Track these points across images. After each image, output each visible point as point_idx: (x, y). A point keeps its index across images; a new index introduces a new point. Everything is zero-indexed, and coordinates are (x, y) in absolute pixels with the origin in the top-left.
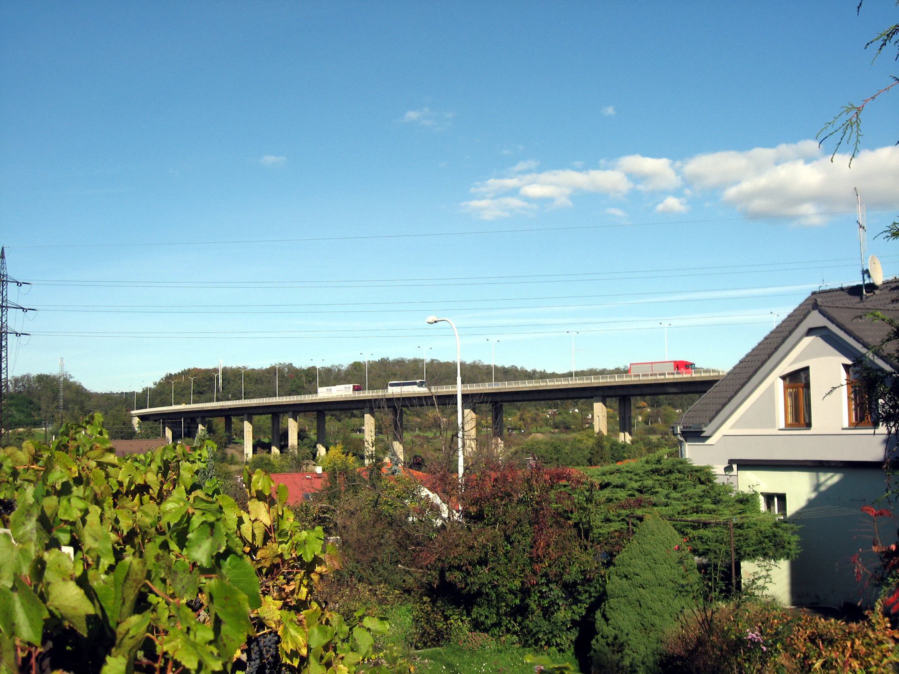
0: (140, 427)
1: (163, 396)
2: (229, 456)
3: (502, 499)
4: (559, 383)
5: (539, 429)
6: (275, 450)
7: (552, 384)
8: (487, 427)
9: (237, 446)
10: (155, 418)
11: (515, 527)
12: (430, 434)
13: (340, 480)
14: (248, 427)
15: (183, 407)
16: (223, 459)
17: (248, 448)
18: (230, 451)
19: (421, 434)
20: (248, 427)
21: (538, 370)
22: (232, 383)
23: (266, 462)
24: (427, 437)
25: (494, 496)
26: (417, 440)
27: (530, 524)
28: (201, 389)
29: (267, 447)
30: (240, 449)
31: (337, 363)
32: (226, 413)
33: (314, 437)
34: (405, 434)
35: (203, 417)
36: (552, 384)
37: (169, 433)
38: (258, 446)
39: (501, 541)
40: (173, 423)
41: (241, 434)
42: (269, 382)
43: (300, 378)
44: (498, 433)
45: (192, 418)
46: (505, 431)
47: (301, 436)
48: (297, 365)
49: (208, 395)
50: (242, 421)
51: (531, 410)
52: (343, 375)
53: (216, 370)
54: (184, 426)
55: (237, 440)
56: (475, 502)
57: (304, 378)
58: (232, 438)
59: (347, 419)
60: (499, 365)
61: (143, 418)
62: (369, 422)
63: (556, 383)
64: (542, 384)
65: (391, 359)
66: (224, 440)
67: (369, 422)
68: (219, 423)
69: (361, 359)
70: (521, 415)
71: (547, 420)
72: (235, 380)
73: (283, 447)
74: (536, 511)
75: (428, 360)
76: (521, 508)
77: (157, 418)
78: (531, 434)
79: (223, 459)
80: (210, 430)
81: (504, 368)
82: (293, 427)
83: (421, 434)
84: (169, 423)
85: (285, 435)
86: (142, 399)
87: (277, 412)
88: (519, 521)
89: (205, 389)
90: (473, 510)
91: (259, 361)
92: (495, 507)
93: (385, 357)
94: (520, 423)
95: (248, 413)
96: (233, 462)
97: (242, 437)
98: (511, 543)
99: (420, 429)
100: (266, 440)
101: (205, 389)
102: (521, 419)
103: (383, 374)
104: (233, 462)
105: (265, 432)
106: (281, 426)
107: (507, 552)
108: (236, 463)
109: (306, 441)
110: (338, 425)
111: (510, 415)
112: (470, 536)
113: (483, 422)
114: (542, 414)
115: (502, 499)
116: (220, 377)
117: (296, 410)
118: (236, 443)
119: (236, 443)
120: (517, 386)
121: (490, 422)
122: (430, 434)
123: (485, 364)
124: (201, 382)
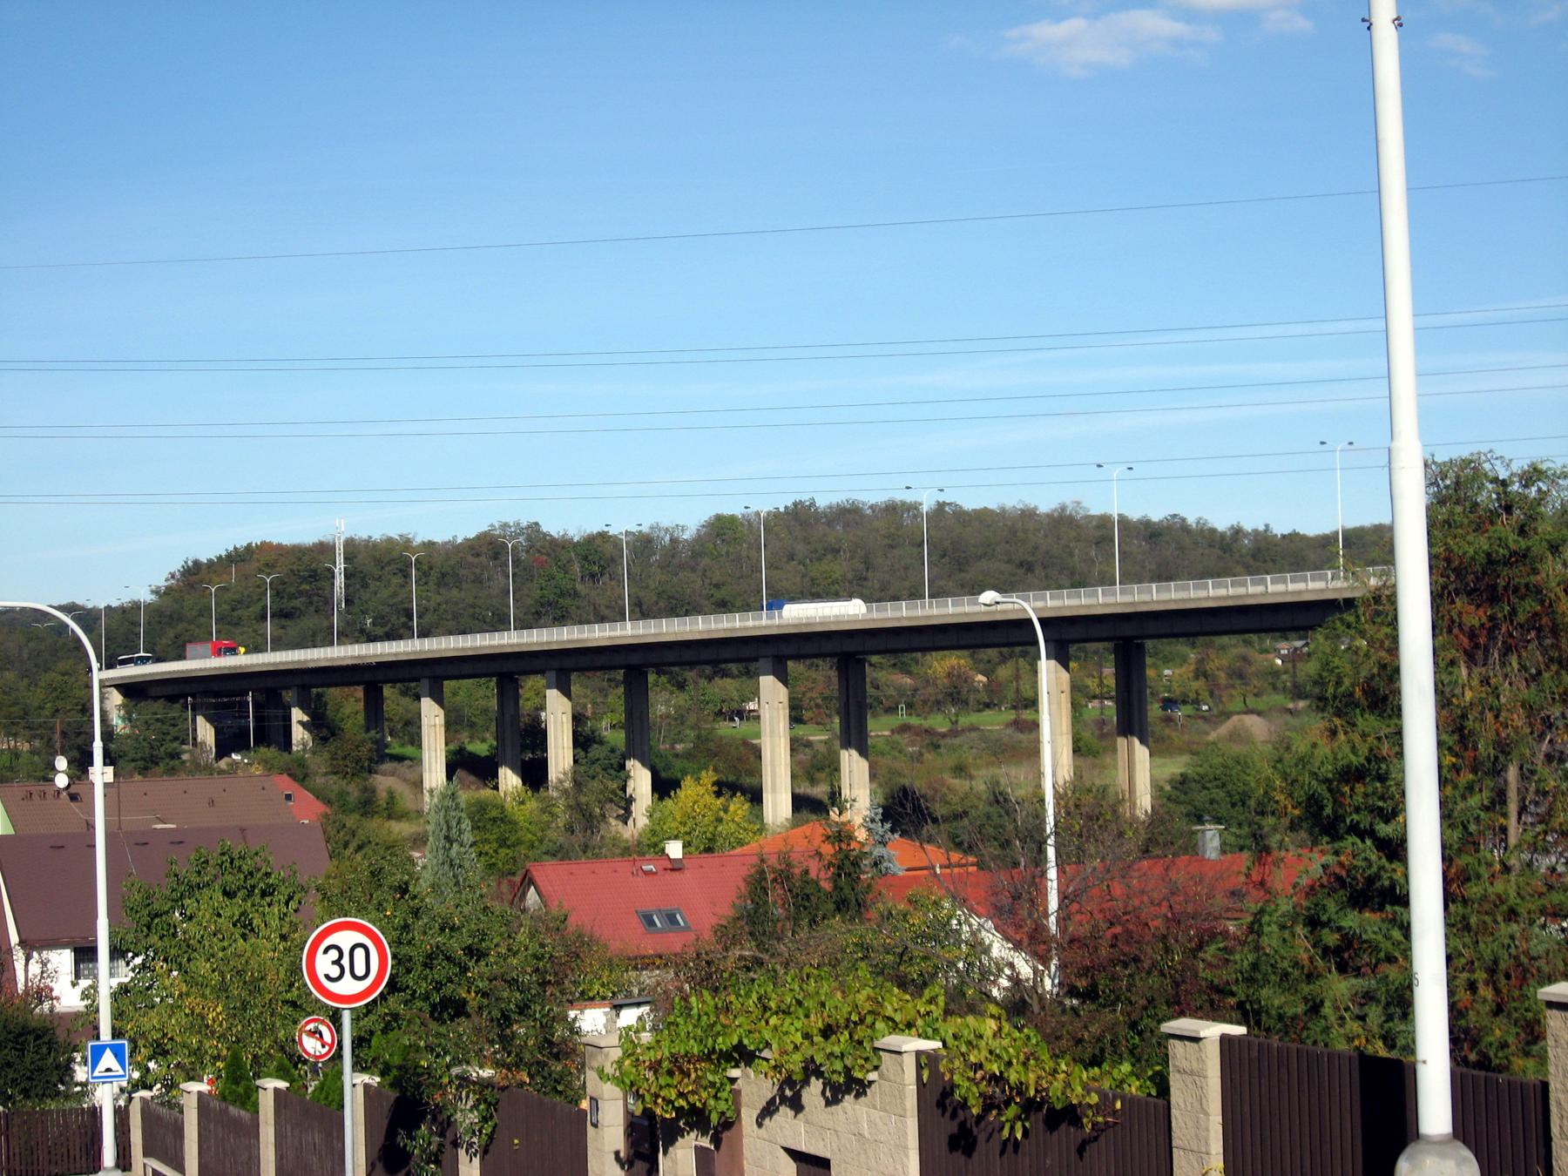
0: (128, 718)
1: (180, 627)
2: (382, 795)
3: (1126, 966)
4: (1301, 586)
5: (1251, 701)
6: (509, 779)
7: (1280, 588)
8: (1101, 697)
9: (401, 768)
10: (169, 690)
11: (1145, 1008)
12: (939, 722)
13: (775, 895)
14: (432, 715)
15: (243, 660)
16: (367, 805)
17: (434, 772)
18: (385, 782)
19: (914, 721)
20: (432, 715)
21: (1248, 526)
22: (373, 585)
23: (494, 813)
24: (929, 732)
25: (1113, 962)
26: (903, 739)
27: (1168, 1004)
28: (288, 605)
29: (484, 770)
30: (411, 775)
31: (666, 521)
32: (368, 677)
33: (617, 738)
34: (872, 724)
35: (304, 689)
36: (1280, 588)
37: (206, 732)
38: (458, 763)
39: (1123, 1031)
40: (216, 706)
41: (412, 731)
42: (478, 580)
43: (564, 569)
44: (1131, 722)
45: (271, 685)
46: (1154, 710)
47: (583, 741)
48: (554, 526)
49: (310, 622)
50: (418, 698)
51: (1228, 650)
52: (685, 555)
53: (325, 549)
54: (249, 712)
55: (396, 749)
56: (1085, 972)
57: (577, 567)
58: (390, 744)
59: (703, 683)
60: (1134, 514)
61: (131, 690)
62: (772, 697)
63: (1292, 587)
64: (1252, 590)
65: (822, 502)
66: (364, 750)
67: (772, 697)
68: (349, 704)
69: (733, 508)
70: (1201, 662)
71: (1275, 673)
72: (387, 578)
73: (535, 775)
74: (1177, 985)
75: (927, 503)
76: (1154, 980)
77: (175, 690)
78: (1228, 715)
79: (367, 805)
80: (321, 725)
81: (1147, 524)
82: (557, 715)
83: (914, 721)
84: (209, 706)
85: (536, 736)
86: (121, 631)
87: (507, 671)
88: (1151, 1001)
89: (297, 603)
90: (1081, 984)
91: (445, 521)
92: (1114, 978)
93: (805, 498)
94: (1196, 685)
95: (430, 675)
96: (392, 811)
97: (416, 740)
98: (1140, 1033)
99: (910, 706)
100: (480, 748)
101: (297, 603)
102: (1200, 673)
103: (800, 548)
104: (392, 811)
105: (472, 725)
106: (526, 706)
107: (1135, 1047)
108: (402, 816)
109: (596, 751)
110: (681, 699)
111: (1167, 661)
112: (1078, 1024)
113: (1092, 684)
114: (1260, 657)
115: (1126, 966)
116: (340, 567)
117: (563, 666)
118: (400, 759)
119: (400, 759)
120: (1182, 595)
121: (1111, 682)
122: (939, 722)
123: (1096, 511)
124: (287, 585)
